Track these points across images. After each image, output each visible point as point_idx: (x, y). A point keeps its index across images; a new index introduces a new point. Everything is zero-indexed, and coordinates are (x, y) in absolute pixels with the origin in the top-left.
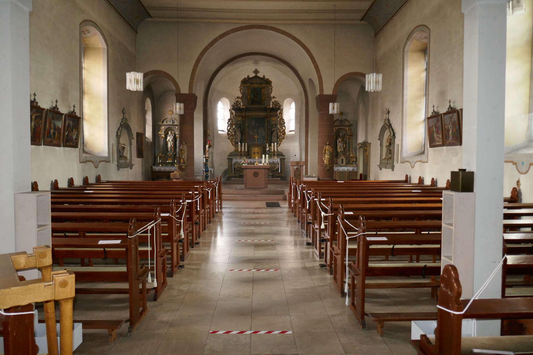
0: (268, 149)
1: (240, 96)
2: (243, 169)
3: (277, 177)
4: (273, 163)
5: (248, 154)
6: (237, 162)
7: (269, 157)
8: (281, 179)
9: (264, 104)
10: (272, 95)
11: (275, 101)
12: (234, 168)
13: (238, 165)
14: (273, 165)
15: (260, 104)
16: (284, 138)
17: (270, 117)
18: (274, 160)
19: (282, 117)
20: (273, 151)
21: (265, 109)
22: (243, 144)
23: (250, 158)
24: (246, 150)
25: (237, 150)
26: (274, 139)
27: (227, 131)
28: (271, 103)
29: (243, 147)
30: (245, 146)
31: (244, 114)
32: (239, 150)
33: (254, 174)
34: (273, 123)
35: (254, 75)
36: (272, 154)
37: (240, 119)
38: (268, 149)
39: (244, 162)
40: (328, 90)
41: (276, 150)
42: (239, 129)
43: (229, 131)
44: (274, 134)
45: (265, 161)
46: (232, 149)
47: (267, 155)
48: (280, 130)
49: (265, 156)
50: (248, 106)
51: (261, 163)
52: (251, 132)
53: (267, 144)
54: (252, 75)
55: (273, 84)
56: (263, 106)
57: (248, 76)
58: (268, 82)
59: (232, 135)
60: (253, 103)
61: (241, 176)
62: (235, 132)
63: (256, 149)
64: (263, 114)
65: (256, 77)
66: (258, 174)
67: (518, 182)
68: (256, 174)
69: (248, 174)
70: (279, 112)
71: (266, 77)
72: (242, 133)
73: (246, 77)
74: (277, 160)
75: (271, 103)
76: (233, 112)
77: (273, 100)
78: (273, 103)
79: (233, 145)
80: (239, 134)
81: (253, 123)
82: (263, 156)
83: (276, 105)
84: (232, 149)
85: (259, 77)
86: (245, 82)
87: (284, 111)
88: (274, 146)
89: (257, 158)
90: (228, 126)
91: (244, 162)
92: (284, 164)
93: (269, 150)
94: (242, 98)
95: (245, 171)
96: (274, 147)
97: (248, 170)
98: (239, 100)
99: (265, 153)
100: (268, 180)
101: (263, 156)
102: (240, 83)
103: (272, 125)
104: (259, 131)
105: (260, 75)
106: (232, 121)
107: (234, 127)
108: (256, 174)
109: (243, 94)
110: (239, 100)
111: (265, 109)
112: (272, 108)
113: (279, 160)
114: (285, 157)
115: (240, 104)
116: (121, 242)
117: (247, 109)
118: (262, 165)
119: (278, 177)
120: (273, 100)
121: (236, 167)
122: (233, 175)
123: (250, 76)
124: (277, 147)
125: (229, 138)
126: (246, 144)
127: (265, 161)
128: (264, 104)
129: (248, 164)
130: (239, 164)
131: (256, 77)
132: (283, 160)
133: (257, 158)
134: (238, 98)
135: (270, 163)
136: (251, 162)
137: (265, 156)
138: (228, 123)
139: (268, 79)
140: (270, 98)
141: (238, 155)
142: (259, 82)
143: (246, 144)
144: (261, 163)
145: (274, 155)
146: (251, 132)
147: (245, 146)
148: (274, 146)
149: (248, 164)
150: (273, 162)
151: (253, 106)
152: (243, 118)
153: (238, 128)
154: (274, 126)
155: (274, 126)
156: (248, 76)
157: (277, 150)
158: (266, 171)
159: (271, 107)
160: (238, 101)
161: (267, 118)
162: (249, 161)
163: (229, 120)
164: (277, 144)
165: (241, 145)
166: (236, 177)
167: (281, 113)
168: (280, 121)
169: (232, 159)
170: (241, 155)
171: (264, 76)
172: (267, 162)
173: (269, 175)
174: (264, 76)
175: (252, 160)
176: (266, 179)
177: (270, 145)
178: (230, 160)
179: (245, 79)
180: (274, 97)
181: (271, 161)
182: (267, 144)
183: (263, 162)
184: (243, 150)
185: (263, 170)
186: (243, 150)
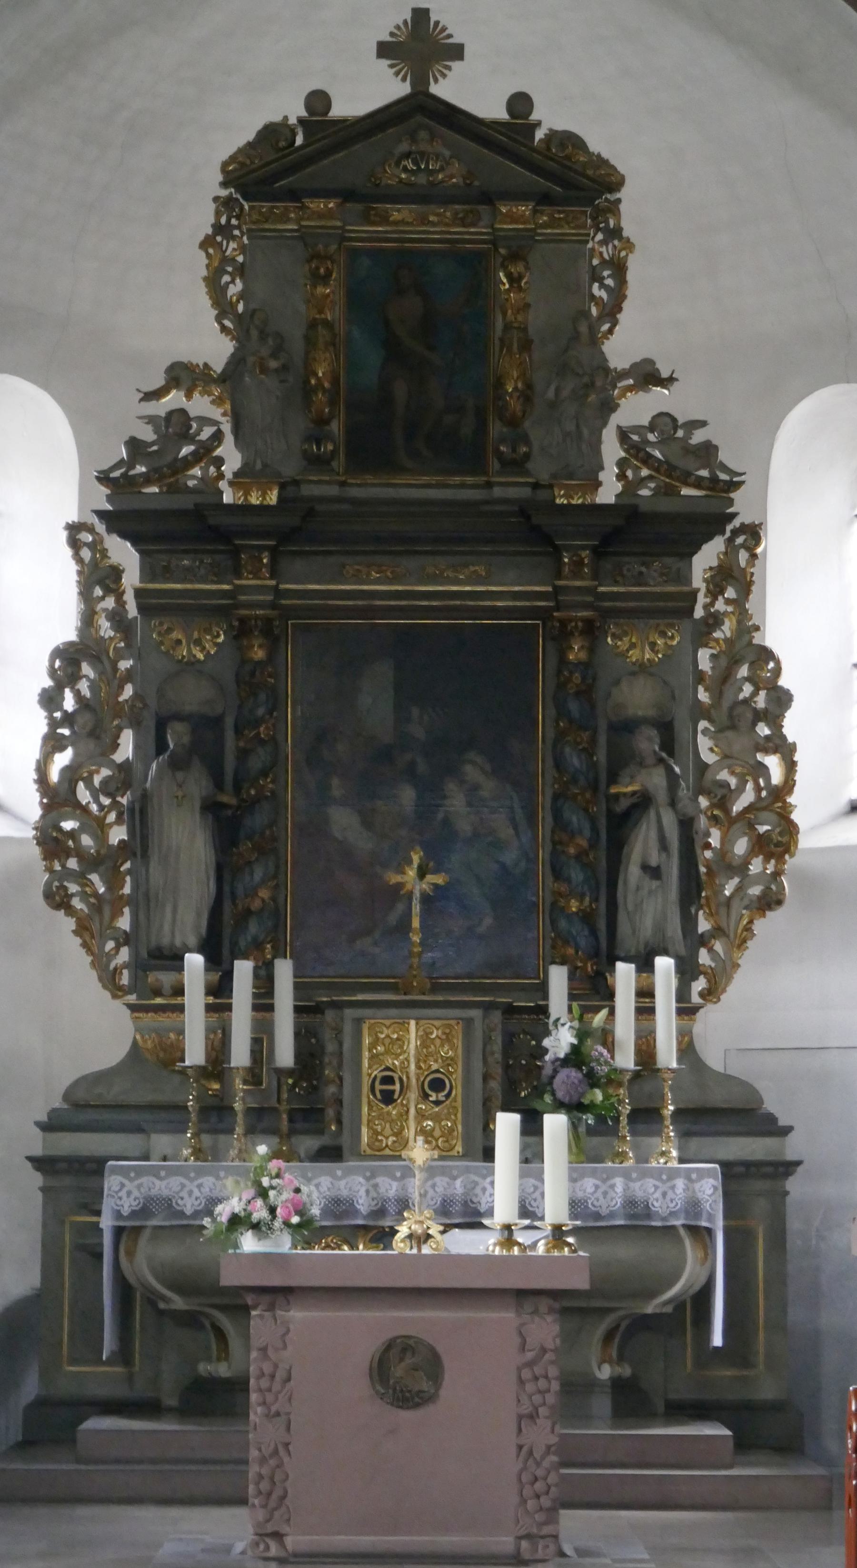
0: (561, 1040)
1: (215, 349)
2: (237, 1303)
3: (681, 1411)
4: (639, 1223)
5: (308, 1108)
6: (167, 1205)
7: (586, 1148)
8: (744, 1445)
9: (516, 465)
10: (621, 349)
11: (664, 421)
12: (125, 1291)
13: (169, 1252)
14: (625, 1252)
15: (470, 457)
16: (770, 901)
17: (592, 631)
18: (647, 1189)
19: (747, 628)
20: (626, 1059)
21: (534, 530)
22: (243, 970)
23: (332, 1153)
24: (285, 1054)
25: (156, 1057)
26: (649, 906)
27: (31, 806)
28: (611, 450)
29: (242, 1017)
30: (263, 1003)
31: (254, 584)
32: (195, 1054)
33: (381, 1369)
34: (638, 698)
35: (385, 87)
36: (615, 1110)
37: (207, 645)
38: (561, 1040)
39: (248, 1202)
40: (535, 520)
41: (667, 1055)
42: (197, 784)
43: (57, 798)
44: (643, 845)
45: (530, 1191)
46: (99, 1030)
47: (555, 1124)
48: (723, 798)
49: (532, 1127)
50: (318, 488)
51: (473, 1219)
52: (343, 821)
53: (558, 978)
54: (367, 89)
55: (634, 209)
56: (511, 490)
57: (318, 101)
58: (576, 183)
59: (105, 861)
60: (369, 451)
61: (217, 1399)
62: (139, 817)
63: (408, 1043)
64: (501, 586)
65: (422, 112)
66: (433, 1366)
67: (140, 418)
68: (405, 1375)
69: (308, 1364)
70: (707, 557)
71: (549, 117)
72: (228, 826)
73: (294, 110)
74: (678, 1180)
75: (611, 450)
76: (124, 554)
77: (636, 409)
78: (634, 448)
79: (110, 980)
80: (188, 841)
81: (375, 700)
82: (507, 1125)
83: (672, 473)
84: (99, 1030)
85: (451, 117)
86: (284, 174)
87: (773, 545)
88: (645, 994)
89: (419, 1153)
90: (53, 743)
91: (248, 1202)
92: (778, 1278)
93: (576, 1057)
94: (230, 380)
95: (260, 1324)
96: (644, 1012)
97: (297, 1315)
98: (200, 405)
99: (522, 1084)
100: (570, 1455)
101: (507, 1125)
102: (211, 183)
103: (625, 727)
104: (456, 802)
105: (473, 89)
106: (111, 679)
107: (126, 748)
108: (405, 1375)
109: (247, 326)
110: (200, 405)
111: (534, 530)
112: (627, 512)
113: (709, 1189)
114: (793, 1148)
115: (205, 453)
116: (131, 864)
117: (296, 530)
118: (481, 1243)
119: (700, 1411)
120: (636, 409)
121: (142, 1267)
122: (101, 1377)
123: (348, 105)
124: (686, 1010)
125: (57, 899)
126: (284, 972)
127: (530, 1191)
128: (516, 465)
129: (307, 1231)
130: (187, 1229)
131: (422, 112)
132: (760, 1186)
133: (419, 1153)
134: (183, 375)
135: (588, 1225)
136: (339, 1207)
137: (532, 1127)
138: (49, 700)
139: (569, 142)
140: (598, 389)
141: (170, 1116)
142: (453, 175)
143: (284, 972)
144: (473, 1219)
145: (646, 1117)
146: (343, 821)
147: (263, 1003)
148: (645, 994)
149: (307, 1231)
150: (638, 1210)
151: (370, 488)
152: (241, 632)
153: (177, 764)
154: (647, 742)
155: (647, 742)
156: (318, 101)
157: (687, 1049)
158: (546, 1330)
159: (608, 492)
160: (177, 425)
161: (561, 636)
162: (319, 1188)
163: (68, 661)
164: (687, 970)
165: (220, 990)
166: (147, 1408)
167: (737, 578)
168: (724, 678)
169: (93, 1168)
170: (216, 1114)
171: (520, 103)
172: (555, 1208)
173: (575, 1389)
174: (520, 103)
175: (353, 1185)
176: (542, 1435)
177: (593, 990)
178: (69, 1178)
179: (272, 134)
180: (648, 376)
181: (611, 1191)
182: (558, 978)
183: (503, 1206)
184: (240, 1055)
185: (505, 1317)
186: (240, 1055)
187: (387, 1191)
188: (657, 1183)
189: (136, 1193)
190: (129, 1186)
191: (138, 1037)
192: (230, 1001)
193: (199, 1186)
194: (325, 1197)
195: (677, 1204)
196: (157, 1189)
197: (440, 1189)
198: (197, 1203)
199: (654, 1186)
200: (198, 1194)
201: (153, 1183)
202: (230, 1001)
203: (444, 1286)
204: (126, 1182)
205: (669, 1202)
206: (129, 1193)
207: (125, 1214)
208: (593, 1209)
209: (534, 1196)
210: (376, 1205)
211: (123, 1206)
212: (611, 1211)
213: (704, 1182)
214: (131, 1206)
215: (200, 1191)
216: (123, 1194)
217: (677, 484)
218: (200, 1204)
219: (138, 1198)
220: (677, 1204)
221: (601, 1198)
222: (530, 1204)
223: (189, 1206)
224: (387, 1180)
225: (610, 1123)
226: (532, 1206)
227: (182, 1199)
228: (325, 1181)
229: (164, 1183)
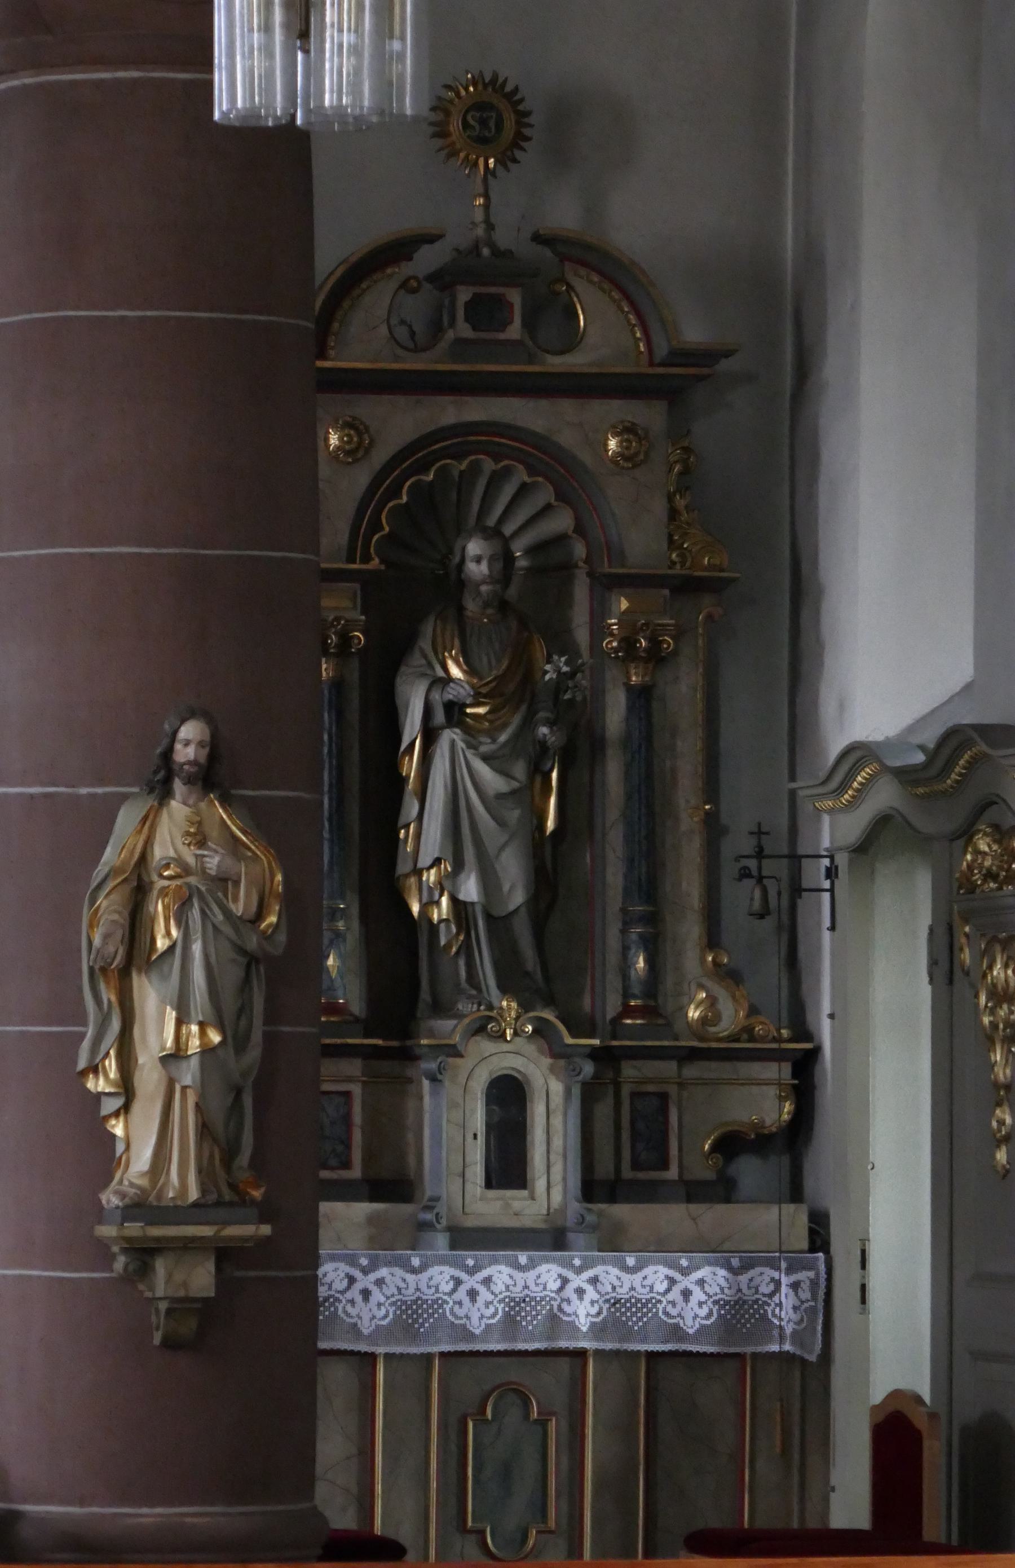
188: (671, 1273)
189: (591, 1293)
191: (661, 1021)
192: (266, 1028)
193: (487, 1281)
194: (607, 1301)
196: (411, 1290)
197: (499, 1287)
198: (594, 1310)
199: (667, 1277)
201: (404, 1280)
202: (266, 1028)
205: (375, 1309)
208: (713, 1319)
211: (467, 1317)
212: (488, 1326)
213: (434, 1271)
215: (489, 1289)
217: (501, 290)
218: (386, 1316)
221: (466, 1300)
226: (564, 1313)
227: (352, 1302)
228: (609, 1274)
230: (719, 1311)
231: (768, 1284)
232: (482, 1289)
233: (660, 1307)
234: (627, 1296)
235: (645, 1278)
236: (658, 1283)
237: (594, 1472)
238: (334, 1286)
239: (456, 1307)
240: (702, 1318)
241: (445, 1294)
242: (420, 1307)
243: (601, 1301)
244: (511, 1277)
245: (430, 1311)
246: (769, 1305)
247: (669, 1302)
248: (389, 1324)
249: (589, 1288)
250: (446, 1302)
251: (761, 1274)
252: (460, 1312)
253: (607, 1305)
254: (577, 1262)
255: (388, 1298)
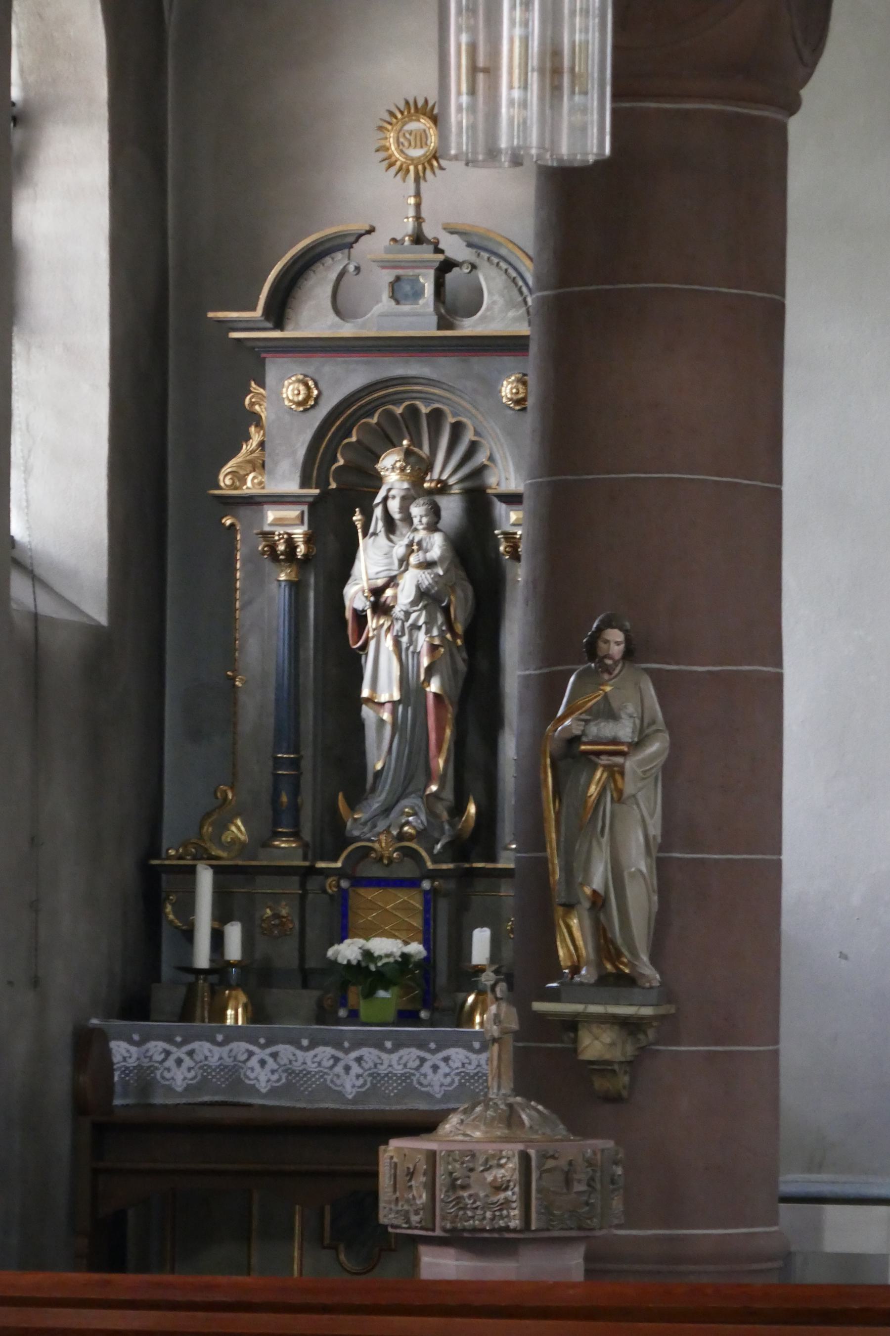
187: (206, 1058)
190: (260, 1054)
193: (446, 1060)
195: (453, 1081)
197: (199, 1057)
200: (192, 1064)
203: (846, 1206)
204: (173, 1049)
205: (442, 1079)
206: (179, 1062)
207: (264, 1091)
209: (250, 1064)
210: (278, 1080)
211: (256, 1079)
214: (185, 1079)
216: (170, 1063)
219: (361, 1075)
220: (453, 1081)
222: (332, 1081)
223: (348, 1088)
224: (207, 1045)
225: (555, 985)
227: (169, 1070)
229: (395, 1057)
230: (287, 1078)
231: (329, 1060)
232: (442, 1065)
233: (415, 1079)
234: (386, 1072)
235: (315, 1056)
236: (239, 1055)
237: (660, 1229)
238: (409, 1065)
239: (422, 1078)
240: (359, 1087)
241: (157, 1062)
242: (390, 1078)
243: (280, 1070)
244: (128, 1051)
245: (214, 1074)
246: (328, 1074)
247: (422, 1075)
248: (198, 1083)
249: (270, 1061)
250: (157, 1068)
251: (409, 1053)
252: (167, 1075)
253: (201, 1071)
254: (179, 1039)
255: (366, 1071)
